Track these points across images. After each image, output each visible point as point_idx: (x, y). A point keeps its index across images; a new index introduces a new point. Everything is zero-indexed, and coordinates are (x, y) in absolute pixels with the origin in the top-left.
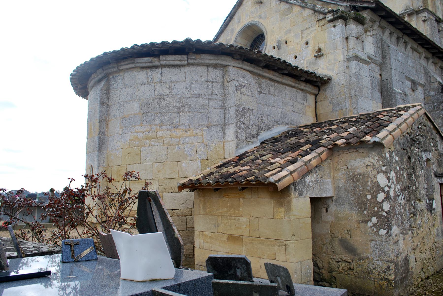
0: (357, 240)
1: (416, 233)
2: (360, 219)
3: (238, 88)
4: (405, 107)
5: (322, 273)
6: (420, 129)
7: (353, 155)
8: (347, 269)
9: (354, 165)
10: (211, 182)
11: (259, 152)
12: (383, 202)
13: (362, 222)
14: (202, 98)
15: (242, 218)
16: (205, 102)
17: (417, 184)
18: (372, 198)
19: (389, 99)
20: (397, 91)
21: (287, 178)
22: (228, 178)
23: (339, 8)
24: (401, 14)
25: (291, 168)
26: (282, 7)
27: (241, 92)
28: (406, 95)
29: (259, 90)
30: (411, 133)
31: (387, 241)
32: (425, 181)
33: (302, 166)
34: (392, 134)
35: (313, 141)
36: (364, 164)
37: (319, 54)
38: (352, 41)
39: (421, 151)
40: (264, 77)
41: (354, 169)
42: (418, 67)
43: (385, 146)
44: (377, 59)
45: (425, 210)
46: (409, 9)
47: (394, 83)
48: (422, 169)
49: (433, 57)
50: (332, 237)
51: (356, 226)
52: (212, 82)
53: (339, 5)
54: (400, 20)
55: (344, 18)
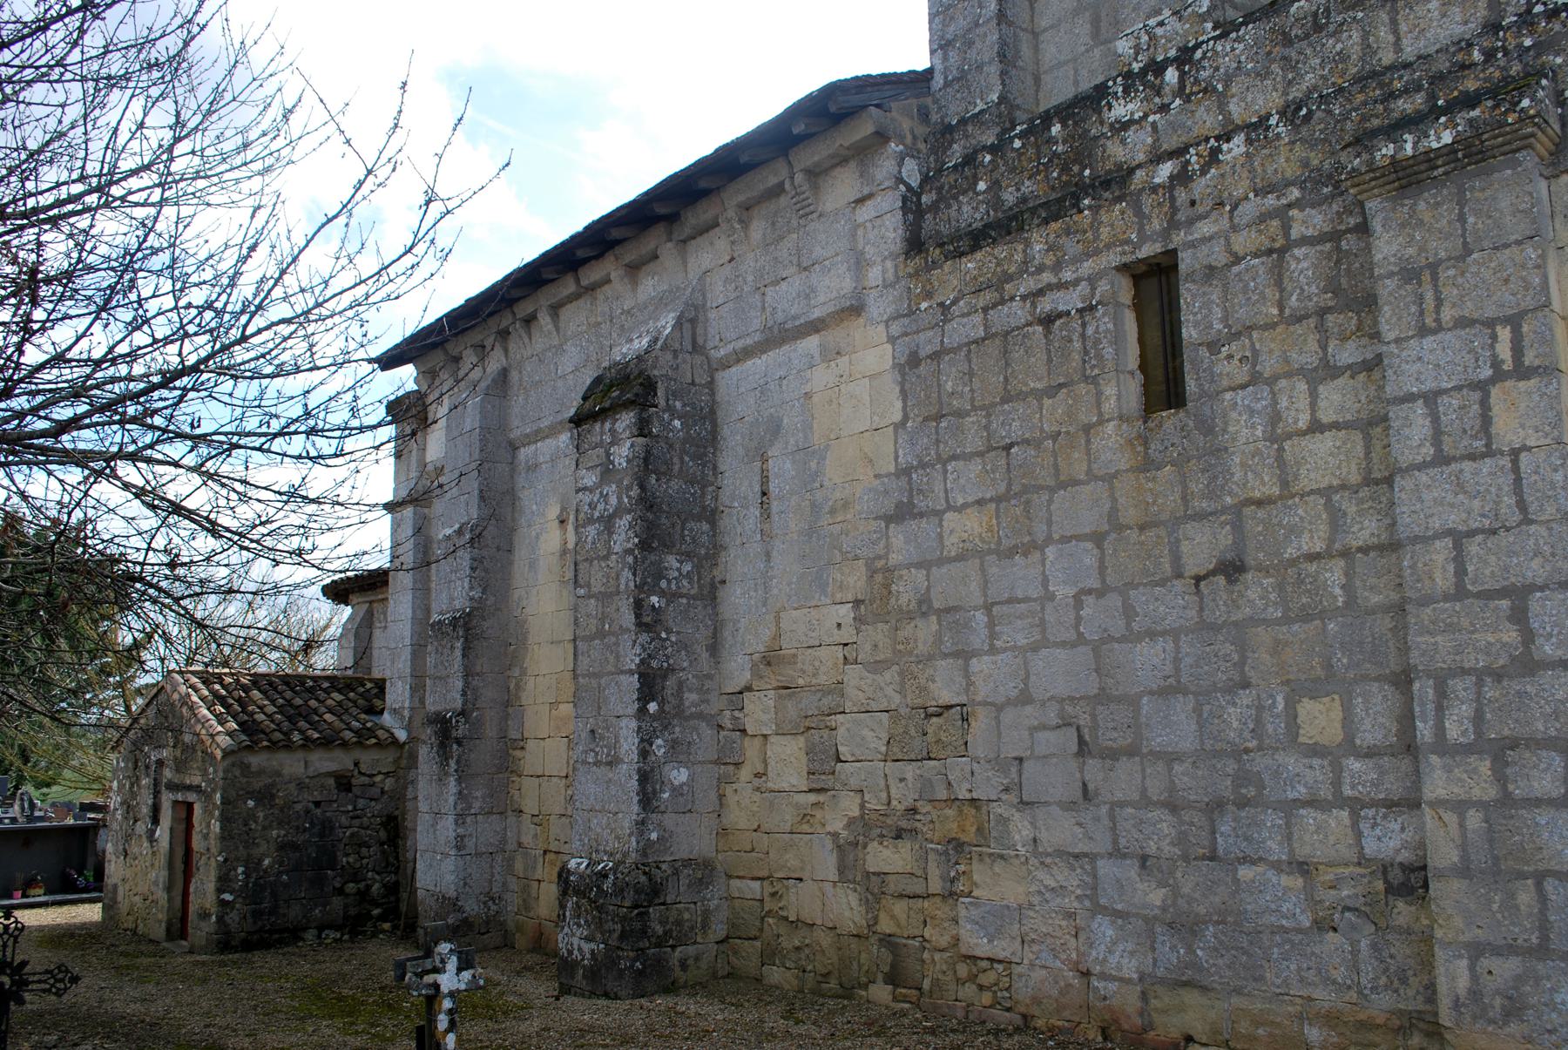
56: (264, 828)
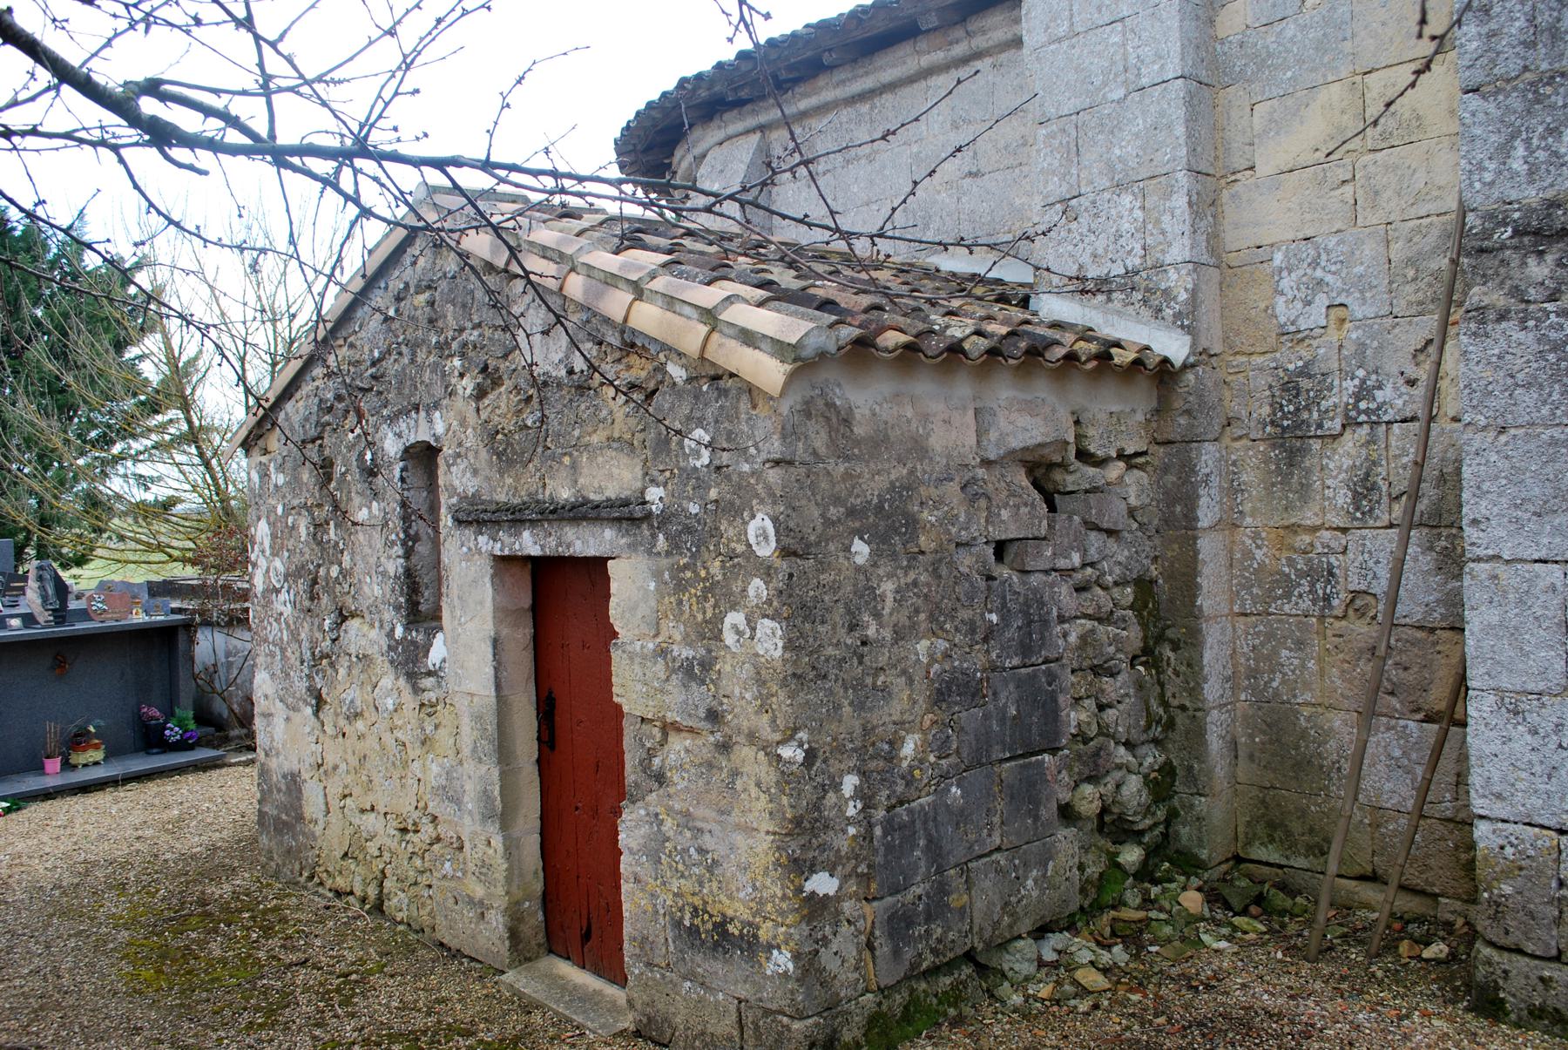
45: (382, 664)
56: (899, 635)
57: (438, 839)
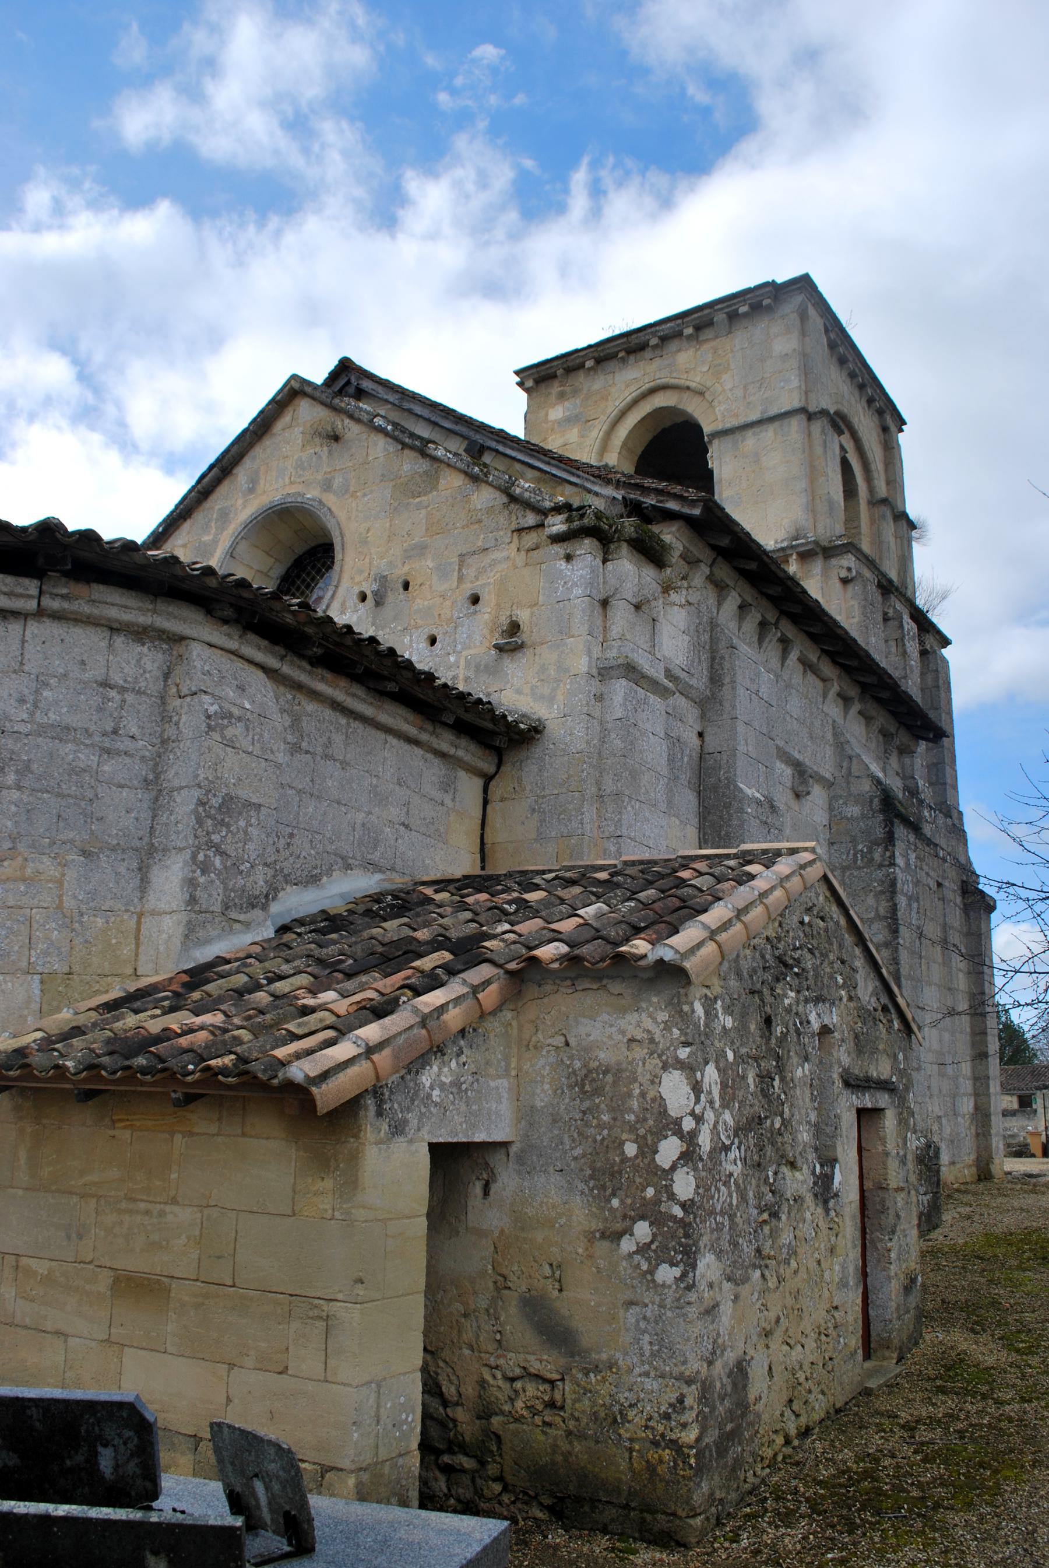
0: (582, 1302)
1: (775, 1279)
2: (596, 1225)
3: (213, 723)
4: (765, 852)
5: (454, 1421)
6: (807, 929)
7: (589, 999)
8: (540, 1407)
9: (588, 1035)
10: (69, 1064)
11: (267, 964)
12: (674, 1168)
13: (603, 1236)
14: (77, 742)
15: (176, 1209)
16: (87, 758)
17: (786, 1110)
18: (641, 1153)
19: (721, 817)
20: (749, 792)
21: (352, 1071)
22: (136, 1055)
23: (590, 500)
24: (778, 550)
25: (372, 1032)
26: (406, 467)
27: (223, 737)
28: (773, 808)
29: (290, 738)
30: (779, 939)
31: (679, 1305)
32: (813, 1099)
33: (411, 1027)
34: (718, 938)
35: (458, 939)
36: (623, 1032)
37: (511, 641)
38: (621, 615)
39: (806, 1001)
40: (314, 695)
41: (588, 1049)
42: (817, 724)
43: (693, 977)
44: (693, 682)
45: (809, 1199)
46: (805, 537)
47: (741, 764)
48: (806, 1059)
49: (861, 700)
50: (498, 1289)
51: (580, 1251)
52: (122, 690)
53: (589, 491)
54: (773, 567)
55: (602, 536)
57: (487, 1310)
